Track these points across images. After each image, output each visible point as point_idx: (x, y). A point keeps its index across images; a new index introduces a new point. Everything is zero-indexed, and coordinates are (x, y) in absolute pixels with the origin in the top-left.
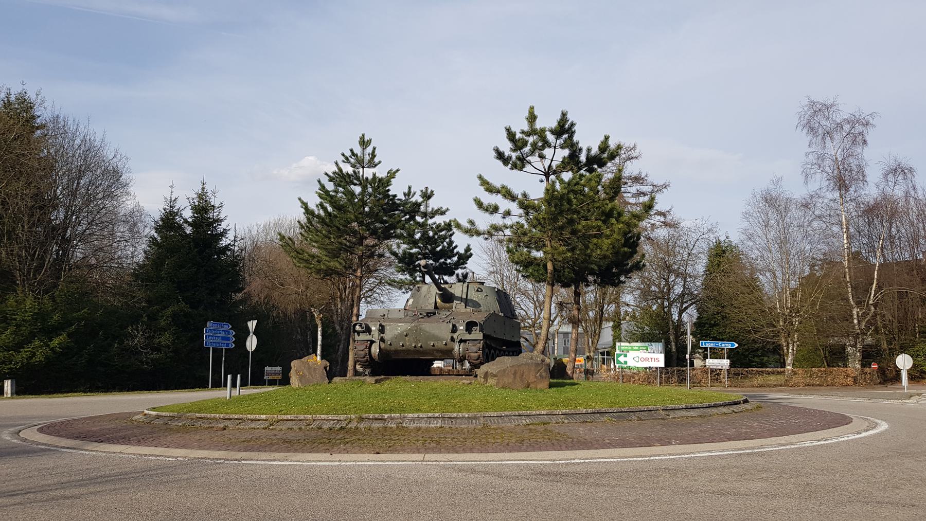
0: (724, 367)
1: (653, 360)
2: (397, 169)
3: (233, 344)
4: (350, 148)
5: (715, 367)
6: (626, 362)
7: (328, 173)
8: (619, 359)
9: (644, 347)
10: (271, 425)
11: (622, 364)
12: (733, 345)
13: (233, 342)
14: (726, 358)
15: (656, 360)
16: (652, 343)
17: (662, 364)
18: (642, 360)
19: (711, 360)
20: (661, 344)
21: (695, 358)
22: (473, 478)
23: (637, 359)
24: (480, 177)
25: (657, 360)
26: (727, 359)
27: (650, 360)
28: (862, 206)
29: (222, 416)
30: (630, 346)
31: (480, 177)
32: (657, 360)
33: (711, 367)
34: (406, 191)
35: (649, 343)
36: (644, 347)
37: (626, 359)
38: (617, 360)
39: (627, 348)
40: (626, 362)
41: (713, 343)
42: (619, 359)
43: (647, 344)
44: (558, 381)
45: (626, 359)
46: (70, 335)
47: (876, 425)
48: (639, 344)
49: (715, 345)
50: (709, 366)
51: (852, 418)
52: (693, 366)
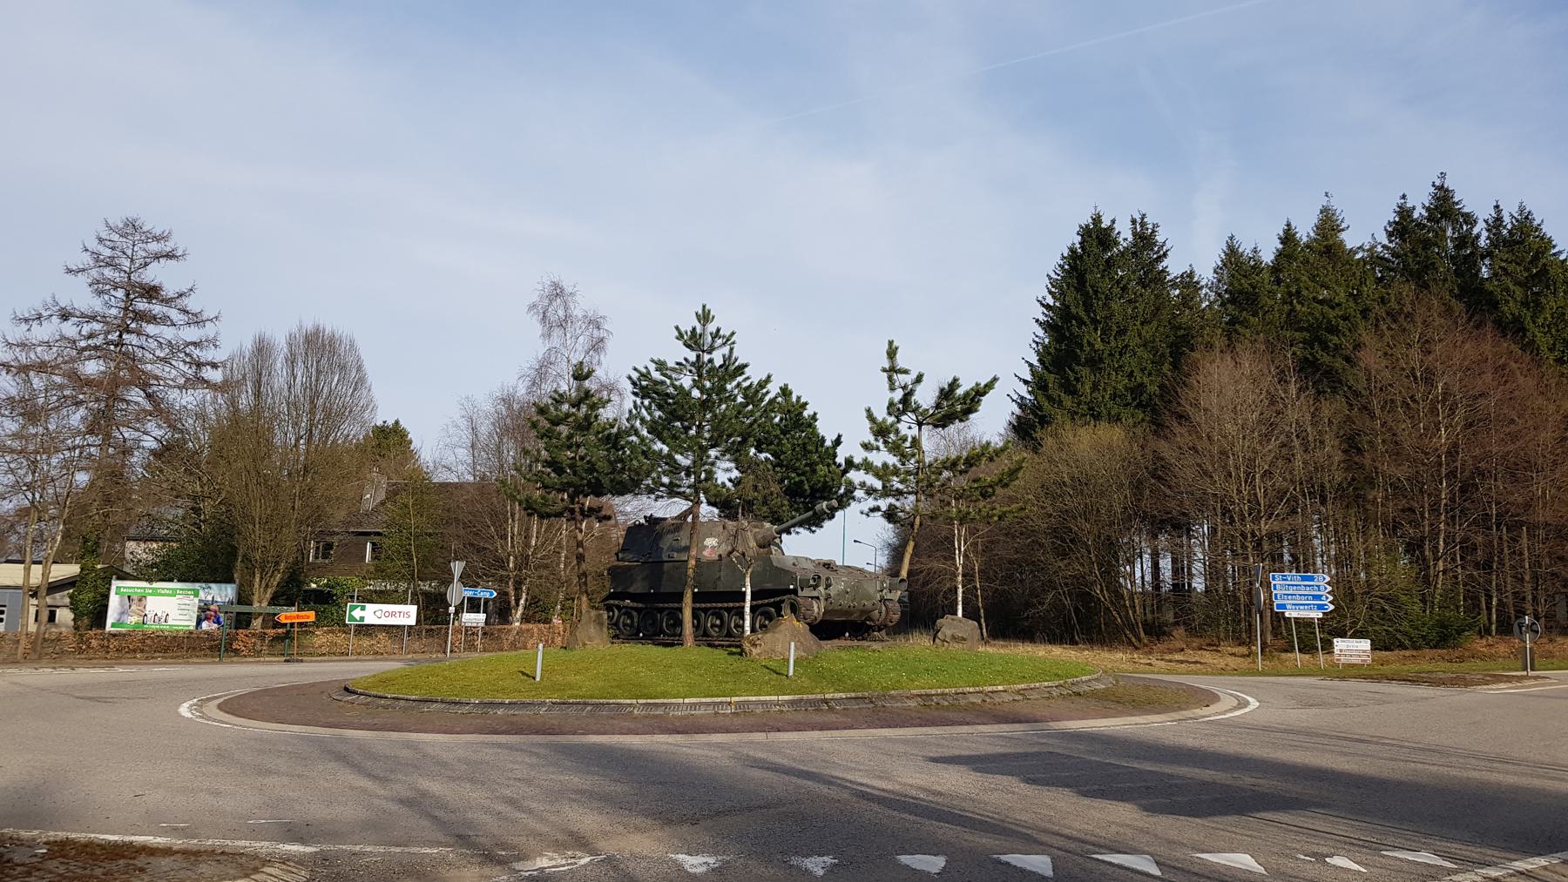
0: (479, 625)
1: (402, 614)
3: (1328, 595)
5: (470, 625)
6: (362, 619)
9: (191, 590)
11: (357, 621)
12: (491, 594)
13: (1329, 593)
18: (387, 614)
19: (468, 614)
20: (234, 586)
21: (58, 607)
22: (883, 794)
23: (378, 614)
24: (868, 411)
25: (407, 614)
26: (1290, 618)
27: (398, 614)
29: (953, 690)
30: (150, 589)
31: (868, 411)
32: (407, 614)
33: (467, 625)
35: (204, 585)
36: (191, 590)
38: (350, 615)
39: (142, 590)
40: (362, 619)
45: (362, 614)
46: (959, 574)
47: (1247, 704)
48: (175, 585)
49: (474, 594)
51: (1219, 694)
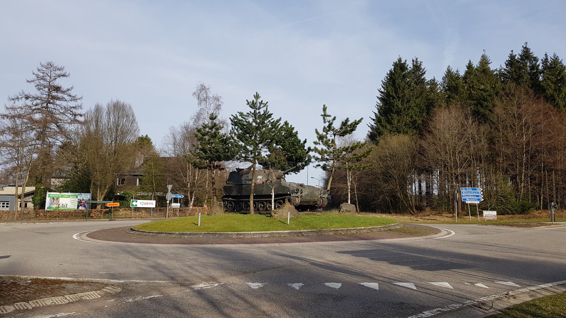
1: (150, 204)
3: (481, 195)
4: (320, 115)
5: (174, 207)
6: (136, 205)
7: (233, 115)
8: (133, 203)
9: (75, 195)
10: (87, 258)
16: (82, 194)
17: (154, 206)
19: (174, 204)
21: (28, 202)
23: (142, 203)
24: (316, 130)
25: (152, 204)
26: (468, 204)
28: (227, 146)
30: (60, 195)
32: (152, 204)
33: (173, 207)
35: (79, 194)
36: (75, 195)
40: (136, 205)
42: (133, 203)
43: (77, 194)
45: (136, 203)
52: (27, 207)
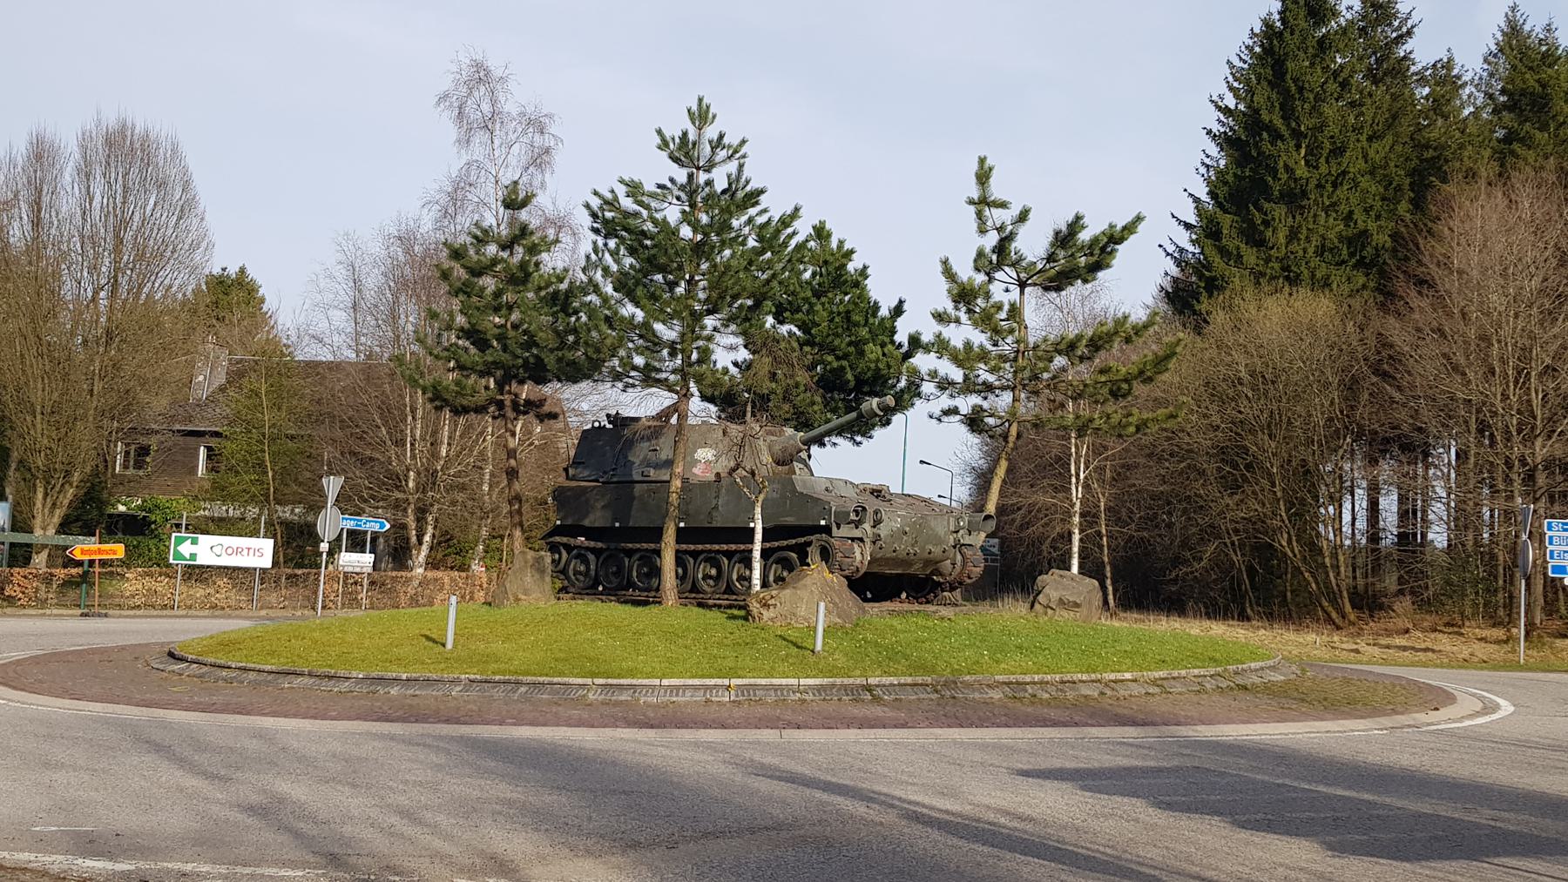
0: (364, 570)
1: (251, 552)
2: (741, 138)
5: (350, 569)
6: (193, 556)
8: (179, 548)
12: (382, 526)
14: (368, 550)
15: (257, 553)
17: (266, 562)
23: (217, 550)
24: (945, 262)
25: (259, 552)
27: (246, 551)
31: (945, 262)
33: (346, 569)
34: (658, 140)
37: (194, 549)
40: (193, 556)
41: (354, 520)
42: (179, 548)
44: (1347, 793)
45: (194, 549)
47: (1496, 708)
50: (344, 566)
51: (1455, 692)
